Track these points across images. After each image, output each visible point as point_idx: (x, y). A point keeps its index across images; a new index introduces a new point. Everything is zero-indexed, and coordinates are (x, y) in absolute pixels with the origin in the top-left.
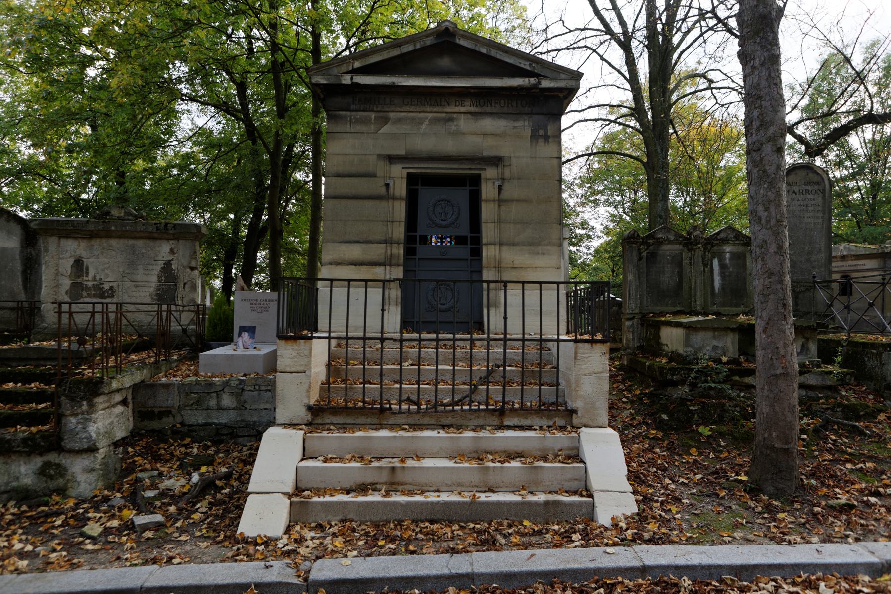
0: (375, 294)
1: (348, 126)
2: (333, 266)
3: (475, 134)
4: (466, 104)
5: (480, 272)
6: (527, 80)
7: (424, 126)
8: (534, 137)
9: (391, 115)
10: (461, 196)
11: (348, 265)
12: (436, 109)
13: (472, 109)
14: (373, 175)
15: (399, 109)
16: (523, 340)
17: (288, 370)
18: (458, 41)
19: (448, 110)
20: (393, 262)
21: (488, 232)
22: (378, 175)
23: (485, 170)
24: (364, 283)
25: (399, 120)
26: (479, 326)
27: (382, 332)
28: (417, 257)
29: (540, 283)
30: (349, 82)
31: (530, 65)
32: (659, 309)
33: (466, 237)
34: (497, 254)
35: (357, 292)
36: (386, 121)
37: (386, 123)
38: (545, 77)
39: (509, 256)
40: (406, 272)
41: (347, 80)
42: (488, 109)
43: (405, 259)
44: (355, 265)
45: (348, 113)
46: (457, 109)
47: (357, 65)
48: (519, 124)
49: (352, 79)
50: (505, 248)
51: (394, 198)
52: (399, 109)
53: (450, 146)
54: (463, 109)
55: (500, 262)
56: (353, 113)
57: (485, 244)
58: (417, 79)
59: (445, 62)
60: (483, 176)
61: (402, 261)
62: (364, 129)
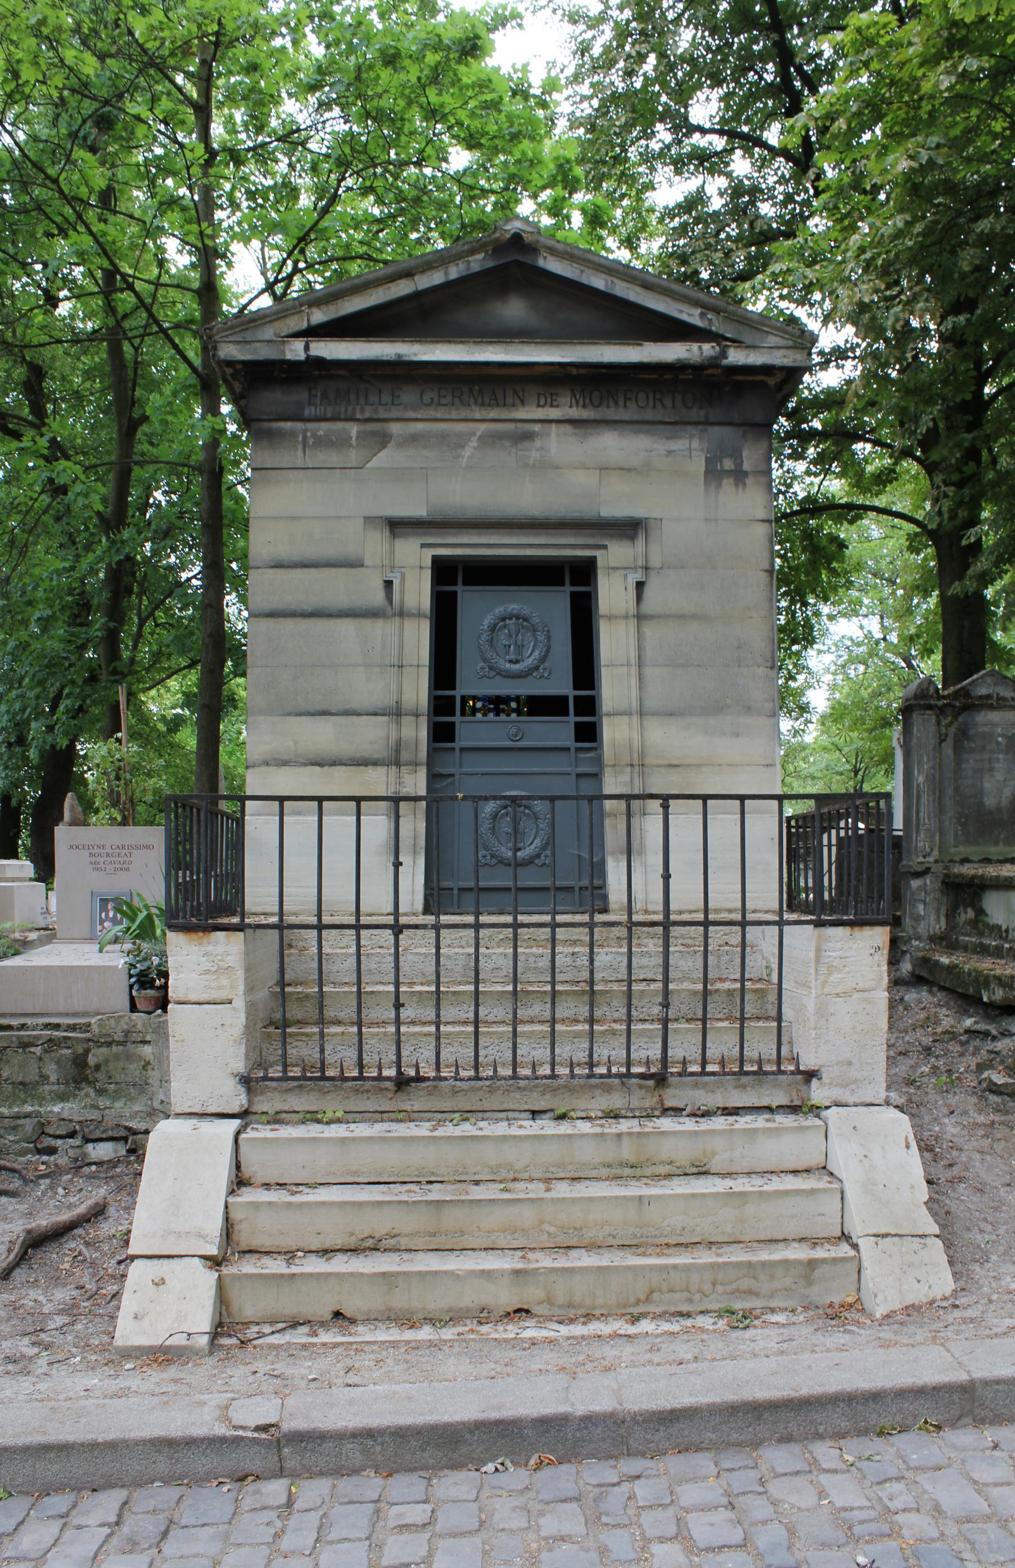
0: (376, 826)
1: (300, 453)
2: (272, 769)
3: (585, 467)
4: (561, 400)
5: (596, 776)
6: (695, 347)
7: (467, 452)
8: (713, 474)
9: (395, 428)
10: (553, 607)
11: (305, 765)
12: (493, 414)
13: (575, 413)
14: (355, 564)
15: (411, 414)
16: (706, 924)
17: (194, 997)
18: (541, 263)
19: (521, 414)
20: (405, 756)
21: (613, 688)
22: (367, 563)
23: (605, 547)
24: (315, 804)
25: (414, 439)
26: (594, 897)
27: (396, 913)
28: (457, 744)
29: (742, 798)
30: (302, 356)
31: (702, 315)
32: (964, 850)
33: (565, 698)
34: (636, 736)
35: (339, 823)
36: (383, 440)
37: (384, 445)
38: (736, 342)
39: (663, 738)
40: (433, 777)
41: (296, 351)
42: (611, 413)
43: (432, 752)
44: (321, 765)
45: (299, 426)
46: (540, 413)
47: (319, 316)
48: (680, 445)
49: (307, 348)
50: (650, 722)
51: (402, 614)
52: (411, 414)
53: (524, 496)
54: (554, 413)
55: (642, 755)
56: (310, 426)
57: (609, 715)
58: (452, 347)
59: (514, 309)
60: (600, 563)
61: (423, 754)
62: (333, 458)
